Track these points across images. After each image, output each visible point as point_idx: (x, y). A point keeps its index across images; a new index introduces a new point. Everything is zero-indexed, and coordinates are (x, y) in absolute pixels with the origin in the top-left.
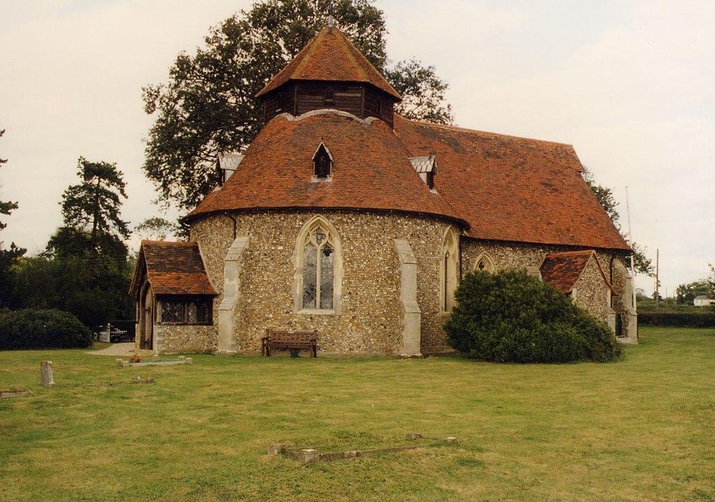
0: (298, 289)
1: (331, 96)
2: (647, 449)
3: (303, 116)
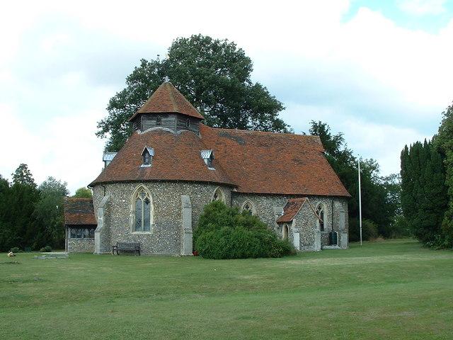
0: (132, 222)
1: (159, 120)
2: (80, 302)
3: (147, 131)
